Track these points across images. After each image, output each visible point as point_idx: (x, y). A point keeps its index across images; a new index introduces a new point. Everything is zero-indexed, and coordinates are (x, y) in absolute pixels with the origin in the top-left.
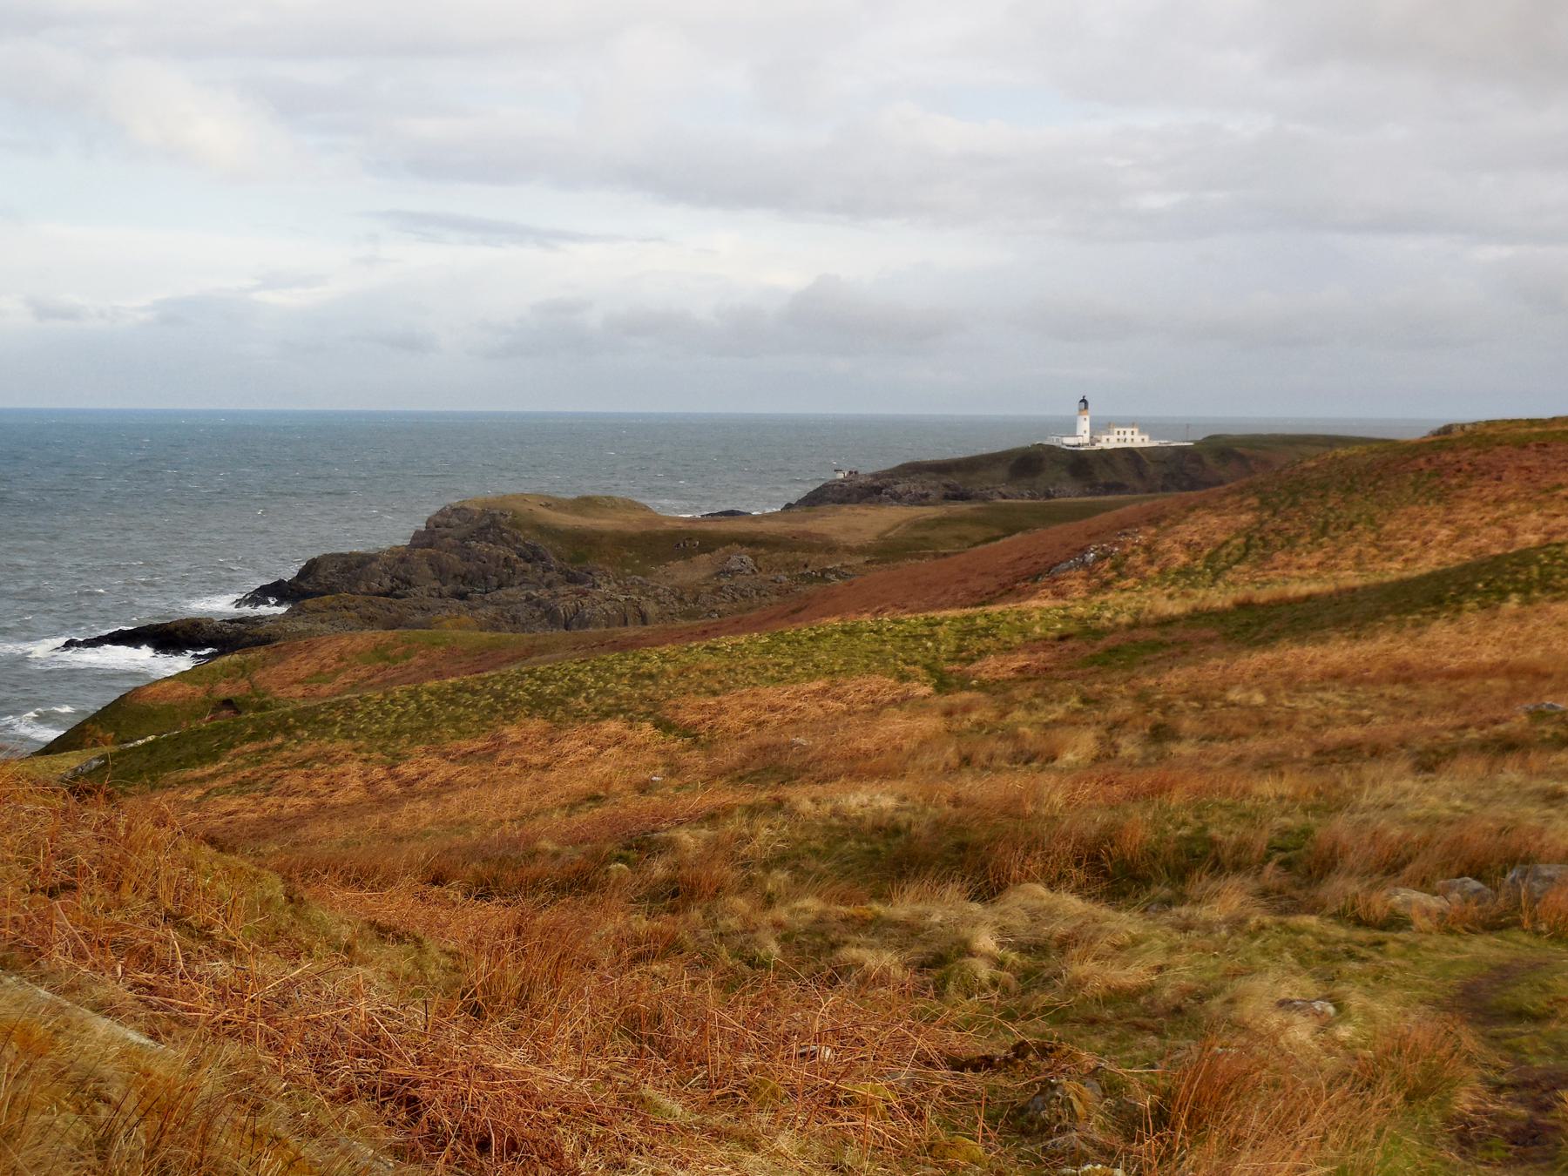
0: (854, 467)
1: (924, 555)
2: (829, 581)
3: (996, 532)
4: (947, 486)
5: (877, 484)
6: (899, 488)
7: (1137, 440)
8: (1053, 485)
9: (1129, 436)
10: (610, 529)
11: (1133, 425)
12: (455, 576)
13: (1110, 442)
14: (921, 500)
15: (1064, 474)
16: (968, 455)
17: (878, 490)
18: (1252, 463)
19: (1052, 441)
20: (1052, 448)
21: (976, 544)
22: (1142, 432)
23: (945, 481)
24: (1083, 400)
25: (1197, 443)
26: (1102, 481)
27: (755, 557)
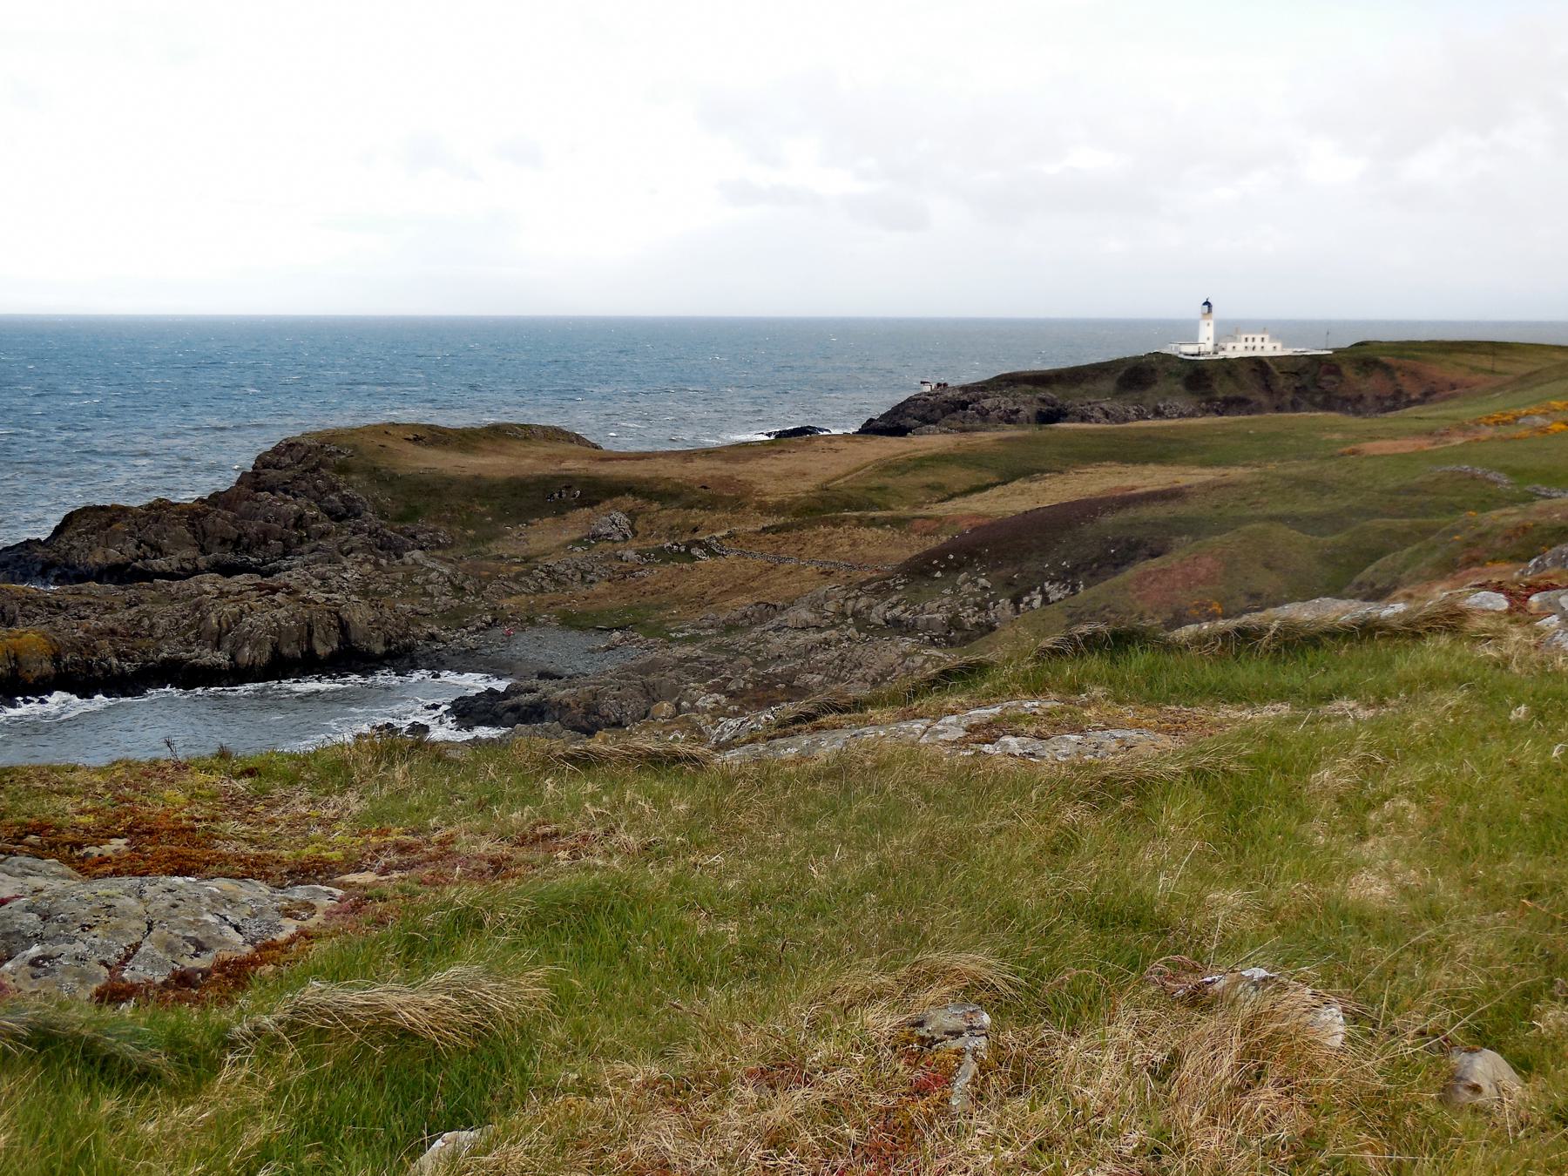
0: (942, 380)
1: (844, 520)
2: (694, 558)
3: (991, 477)
4: (1043, 401)
5: (965, 397)
6: (987, 403)
7: (1269, 348)
8: (1164, 400)
9: (1258, 343)
10: (500, 475)
11: (1264, 331)
12: (224, 542)
13: (1236, 350)
14: (1010, 418)
15: (1179, 387)
16: (1071, 364)
17: (964, 405)
18: (1398, 374)
19: (1170, 349)
20: (1168, 358)
21: (952, 497)
22: (1275, 337)
23: (1042, 395)
24: (1207, 303)
25: (1337, 351)
26: (1221, 395)
27: (632, 515)
